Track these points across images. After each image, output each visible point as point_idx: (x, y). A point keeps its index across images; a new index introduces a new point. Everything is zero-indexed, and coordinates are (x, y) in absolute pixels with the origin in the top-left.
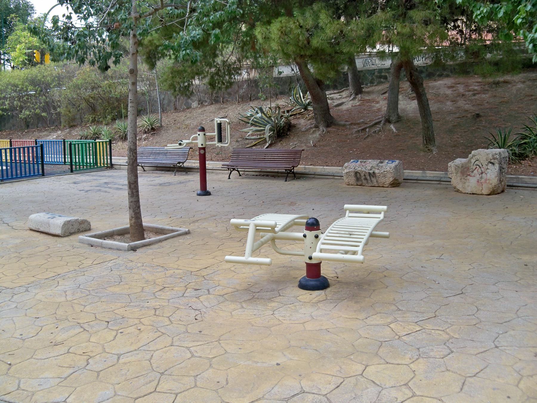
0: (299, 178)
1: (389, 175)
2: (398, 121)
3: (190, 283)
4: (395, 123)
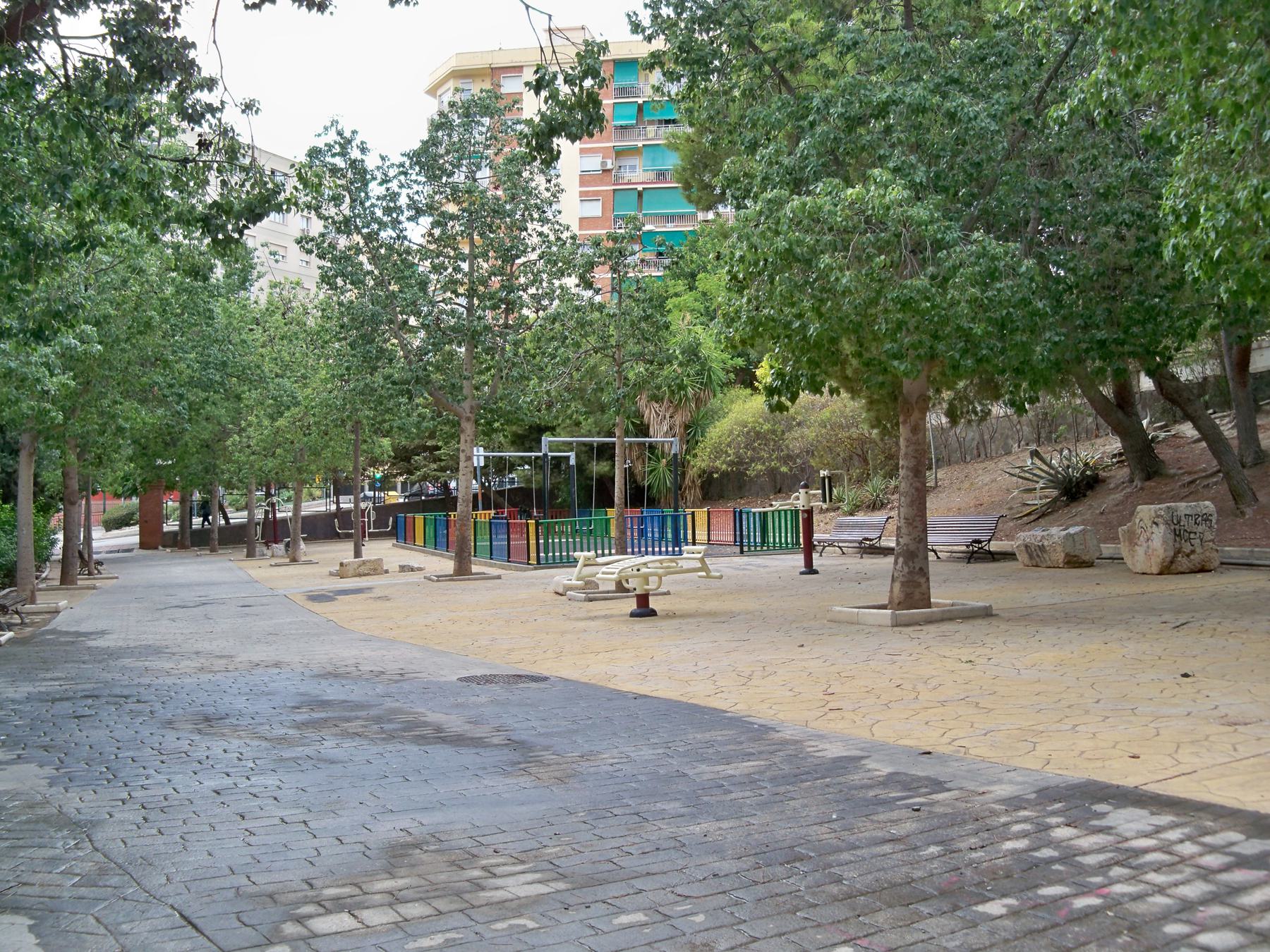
0: (998, 560)
1: (1059, 549)
2: (1256, 465)
3: (755, 939)
4: (1251, 467)
